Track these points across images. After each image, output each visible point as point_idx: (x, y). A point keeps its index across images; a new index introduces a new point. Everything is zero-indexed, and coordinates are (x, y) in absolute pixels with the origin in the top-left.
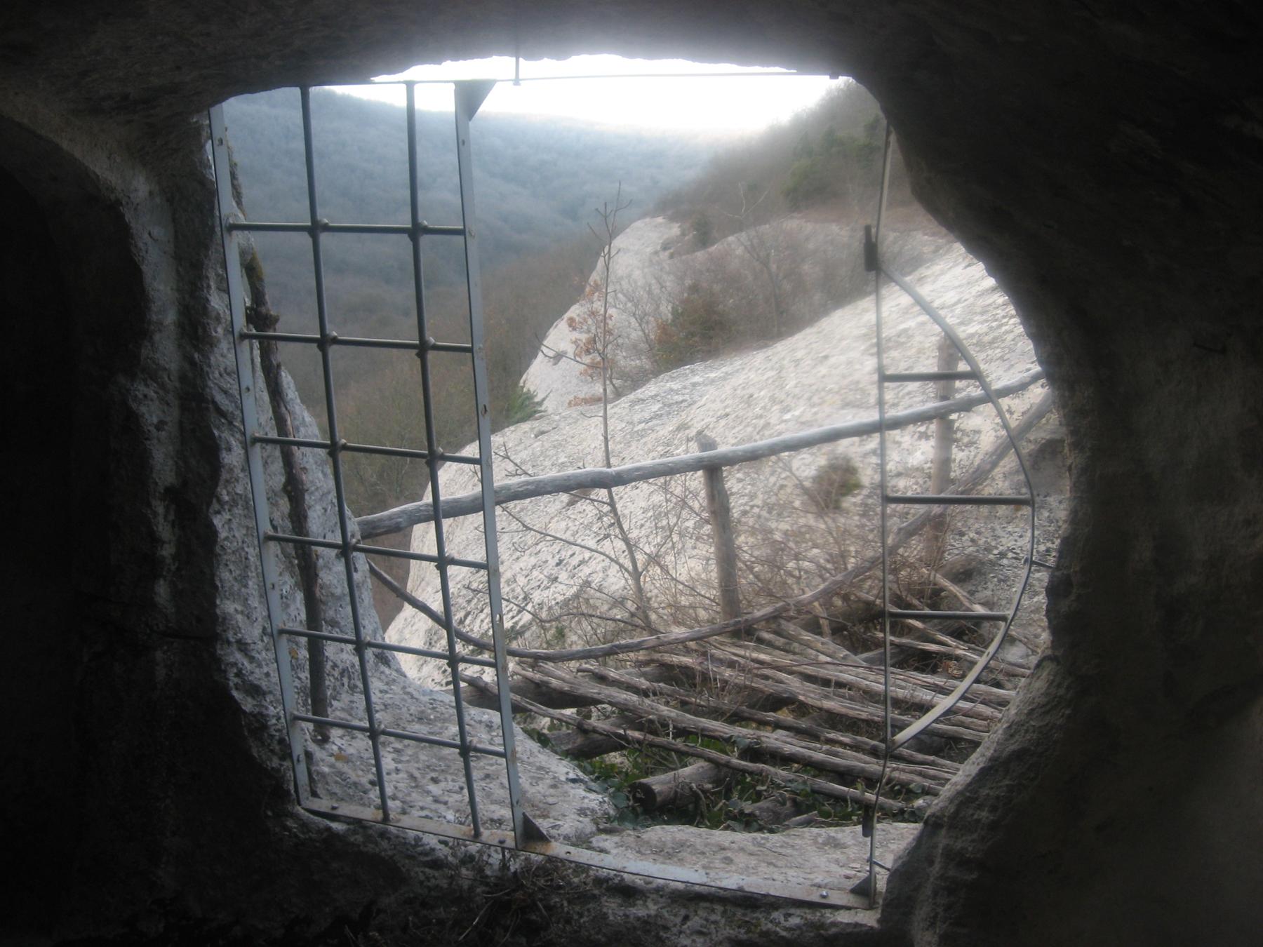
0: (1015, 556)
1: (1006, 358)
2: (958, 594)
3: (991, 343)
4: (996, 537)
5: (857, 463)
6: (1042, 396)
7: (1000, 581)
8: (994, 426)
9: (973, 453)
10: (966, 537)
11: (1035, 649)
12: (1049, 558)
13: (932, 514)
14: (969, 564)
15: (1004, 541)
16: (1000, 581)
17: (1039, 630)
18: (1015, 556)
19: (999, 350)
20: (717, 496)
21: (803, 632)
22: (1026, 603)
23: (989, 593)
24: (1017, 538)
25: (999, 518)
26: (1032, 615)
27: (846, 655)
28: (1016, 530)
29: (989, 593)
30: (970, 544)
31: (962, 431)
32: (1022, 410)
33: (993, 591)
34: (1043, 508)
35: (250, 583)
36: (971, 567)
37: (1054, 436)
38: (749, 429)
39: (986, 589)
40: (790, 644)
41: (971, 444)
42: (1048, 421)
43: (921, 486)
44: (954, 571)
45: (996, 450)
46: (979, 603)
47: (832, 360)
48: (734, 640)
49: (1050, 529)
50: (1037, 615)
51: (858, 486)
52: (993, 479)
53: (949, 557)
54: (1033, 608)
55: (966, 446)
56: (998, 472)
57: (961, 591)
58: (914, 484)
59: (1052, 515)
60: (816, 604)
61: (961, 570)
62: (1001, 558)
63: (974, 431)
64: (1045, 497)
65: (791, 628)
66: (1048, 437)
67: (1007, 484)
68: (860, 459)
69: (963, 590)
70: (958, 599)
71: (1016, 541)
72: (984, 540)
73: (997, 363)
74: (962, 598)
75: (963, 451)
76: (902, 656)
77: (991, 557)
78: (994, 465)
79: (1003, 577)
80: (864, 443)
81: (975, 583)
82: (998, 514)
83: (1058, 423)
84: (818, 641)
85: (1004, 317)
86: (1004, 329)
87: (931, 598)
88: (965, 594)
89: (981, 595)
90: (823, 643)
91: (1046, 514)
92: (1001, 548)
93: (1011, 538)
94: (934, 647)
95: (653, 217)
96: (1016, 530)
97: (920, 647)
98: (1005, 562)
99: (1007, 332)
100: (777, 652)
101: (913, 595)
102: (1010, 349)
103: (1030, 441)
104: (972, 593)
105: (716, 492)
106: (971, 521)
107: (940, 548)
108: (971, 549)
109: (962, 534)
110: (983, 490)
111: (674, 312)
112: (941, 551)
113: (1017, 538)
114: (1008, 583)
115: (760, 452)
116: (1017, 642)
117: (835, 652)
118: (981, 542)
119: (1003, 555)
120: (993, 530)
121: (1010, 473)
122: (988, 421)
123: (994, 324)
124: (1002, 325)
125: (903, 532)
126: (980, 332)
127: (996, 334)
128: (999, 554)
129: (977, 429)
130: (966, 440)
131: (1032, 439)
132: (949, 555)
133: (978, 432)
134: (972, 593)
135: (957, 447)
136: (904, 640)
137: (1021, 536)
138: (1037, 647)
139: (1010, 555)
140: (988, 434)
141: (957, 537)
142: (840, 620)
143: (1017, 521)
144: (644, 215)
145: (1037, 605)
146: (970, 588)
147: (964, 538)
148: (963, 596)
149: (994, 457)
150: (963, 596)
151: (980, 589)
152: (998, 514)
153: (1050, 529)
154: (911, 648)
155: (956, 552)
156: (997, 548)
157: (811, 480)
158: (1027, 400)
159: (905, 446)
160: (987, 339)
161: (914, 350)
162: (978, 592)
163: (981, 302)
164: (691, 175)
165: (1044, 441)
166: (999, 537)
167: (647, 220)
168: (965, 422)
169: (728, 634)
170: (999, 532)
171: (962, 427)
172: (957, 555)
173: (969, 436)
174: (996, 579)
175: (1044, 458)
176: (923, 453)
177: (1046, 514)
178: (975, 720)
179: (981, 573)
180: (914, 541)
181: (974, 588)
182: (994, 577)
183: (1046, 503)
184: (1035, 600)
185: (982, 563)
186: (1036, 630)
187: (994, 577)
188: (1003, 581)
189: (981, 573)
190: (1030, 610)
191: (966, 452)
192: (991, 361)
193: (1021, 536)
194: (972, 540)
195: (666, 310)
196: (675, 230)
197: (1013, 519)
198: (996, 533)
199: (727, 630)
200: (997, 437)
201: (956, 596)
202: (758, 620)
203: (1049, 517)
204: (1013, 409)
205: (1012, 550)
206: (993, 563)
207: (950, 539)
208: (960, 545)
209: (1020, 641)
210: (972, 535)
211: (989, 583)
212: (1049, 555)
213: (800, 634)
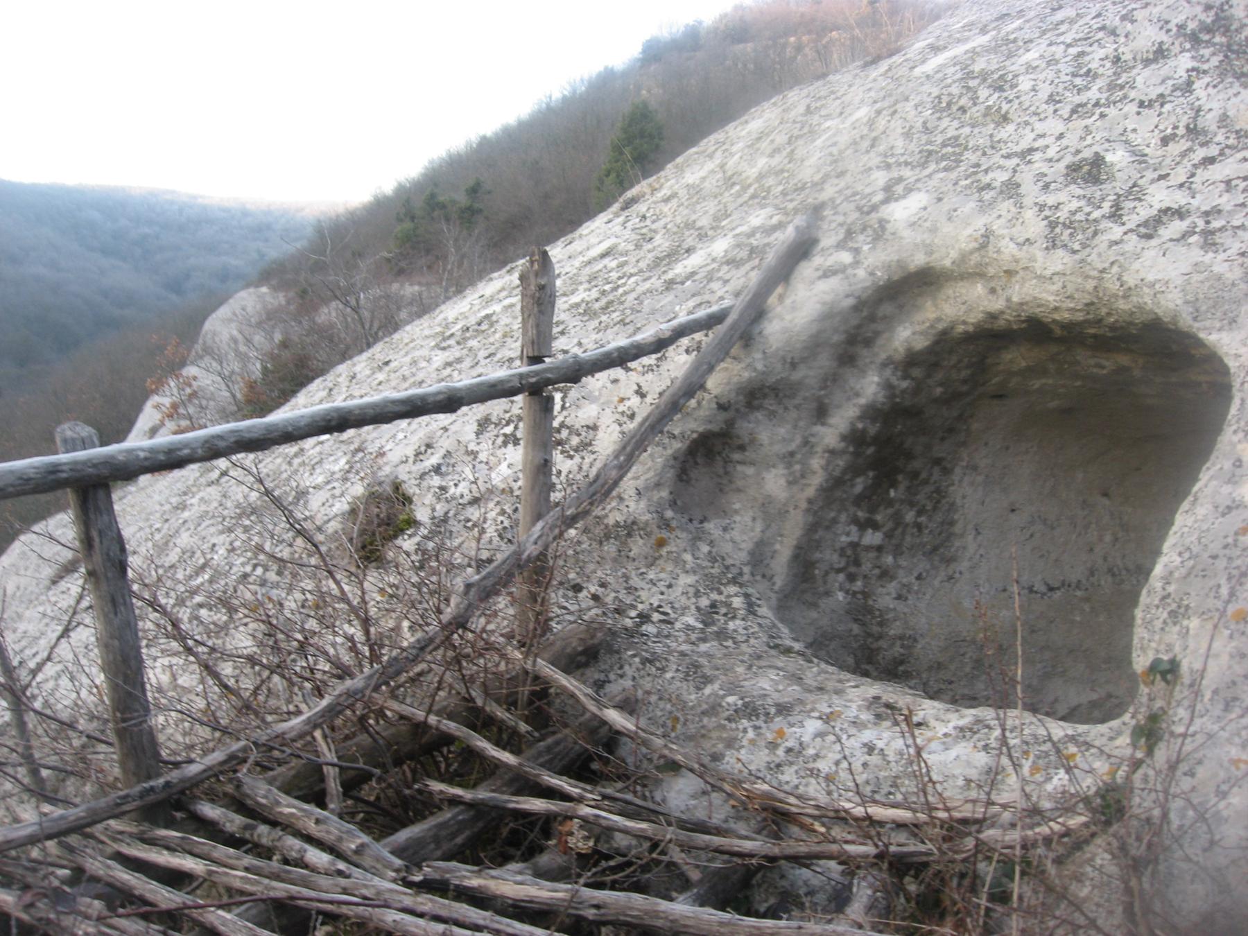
0: (663, 617)
1: (627, 321)
2: (577, 692)
3: (604, 309)
4: (631, 590)
5: (410, 488)
6: (687, 366)
7: (645, 661)
8: (618, 416)
9: (587, 460)
10: (585, 593)
11: (719, 784)
12: (716, 616)
13: (525, 556)
14: (593, 637)
15: (644, 595)
16: (645, 661)
17: (720, 746)
18: (663, 617)
19: (617, 314)
20: (97, 540)
21: (284, 799)
22: (693, 697)
23: (628, 683)
24: (664, 589)
25: (634, 560)
26: (706, 720)
27: (362, 845)
28: (662, 575)
29: (628, 683)
30: (592, 603)
31: (568, 428)
32: (659, 390)
33: (634, 678)
34: (700, 539)
35: (650, 598)
36: (596, 641)
37: (709, 427)
38: (279, 460)
39: (621, 676)
40: (253, 828)
41: (585, 445)
42: (699, 403)
43: (509, 517)
44: (569, 650)
45: (624, 448)
46: (614, 707)
47: (392, 365)
48: (145, 827)
49: (712, 571)
50: (714, 719)
51: (413, 523)
52: (621, 499)
53: (559, 627)
54: (705, 706)
55: (576, 451)
56: (628, 486)
57: (582, 686)
58: (499, 514)
59: (714, 550)
60: (318, 734)
61: (580, 649)
62: (642, 623)
63: (588, 427)
64: (701, 522)
65: (261, 790)
66: (701, 429)
67: (643, 504)
68: (414, 482)
69: (584, 683)
70: (578, 700)
71: (662, 593)
72: (613, 595)
73: (616, 328)
74: (582, 698)
75: (571, 457)
76: (480, 824)
77: (628, 623)
78: (624, 469)
79: (648, 655)
80: (421, 457)
81: (603, 667)
82: (631, 554)
83: (715, 406)
84: (308, 814)
85: (620, 278)
86: (621, 290)
87: (530, 703)
88: (589, 691)
89: (617, 687)
90: (318, 821)
91: (705, 549)
92: (640, 607)
93: (654, 589)
94: (537, 805)
95: (257, 286)
96: (662, 575)
97: (512, 805)
98: (649, 629)
99: (626, 293)
100: (223, 851)
101: (498, 702)
102: (632, 309)
103: (674, 437)
104: (599, 685)
105: (95, 534)
106: (591, 567)
107: (538, 614)
108: (594, 611)
109: (577, 588)
110: (606, 516)
111: (265, 370)
112: (544, 626)
113: (664, 589)
114: (658, 664)
115: (186, 451)
116: (684, 770)
117: (340, 839)
118: (609, 599)
119: (644, 618)
120: (626, 578)
121: (647, 488)
122: (608, 411)
123: (607, 287)
124: (618, 287)
125: (473, 591)
126: (587, 299)
127: (611, 297)
128: (640, 615)
129: (591, 425)
130: (575, 441)
131: (676, 432)
132: (558, 623)
133: (594, 428)
134: (599, 685)
135: (562, 452)
136: (482, 794)
137: (670, 586)
138: (723, 780)
139: (656, 617)
140: (609, 430)
141: (571, 594)
142: (361, 765)
143: (661, 562)
144: (247, 286)
145: (712, 699)
146: (597, 676)
147: (581, 595)
148: (586, 695)
149: (622, 458)
150: (586, 695)
151: (612, 676)
152: (631, 554)
153: (712, 571)
154: (496, 807)
155: (571, 618)
156: (633, 607)
157: (339, 519)
158: (666, 374)
159: (483, 456)
160: (597, 306)
161: (498, 336)
162: (609, 682)
163: (587, 270)
164: (291, 248)
165: (695, 436)
166: (636, 589)
167: (252, 290)
168: (573, 415)
169: (133, 815)
170: (635, 581)
171: (568, 422)
172: (571, 622)
173: (579, 435)
174: (637, 660)
175: (696, 463)
176: (510, 466)
177: (705, 549)
178: (603, 814)
179: (611, 651)
180: (501, 602)
181: (602, 677)
182: (634, 656)
183: (703, 532)
184: (708, 690)
185: (612, 633)
186: (714, 746)
187: (634, 656)
188: (650, 662)
189: (611, 651)
190: (699, 710)
191: (577, 459)
192: (606, 328)
193: (670, 586)
194: (595, 597)
195: (256, 369)
196: (281, 298)
197: (656, 559)
198: (631, 582)
199: (126, 808)
200: (623, 433)
201: (573, 696)
202: (195, 782)
203: (710, 552)
204: (645, 389)
205: (657, 609)
206: (631, 633)
207: (556, 597)
208: (576, 607)
209: (692, 770)
210: (593, 589)
211: (627, 667)
212: (717, 613)
213: (278, 803)
